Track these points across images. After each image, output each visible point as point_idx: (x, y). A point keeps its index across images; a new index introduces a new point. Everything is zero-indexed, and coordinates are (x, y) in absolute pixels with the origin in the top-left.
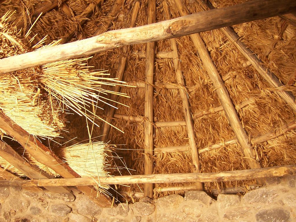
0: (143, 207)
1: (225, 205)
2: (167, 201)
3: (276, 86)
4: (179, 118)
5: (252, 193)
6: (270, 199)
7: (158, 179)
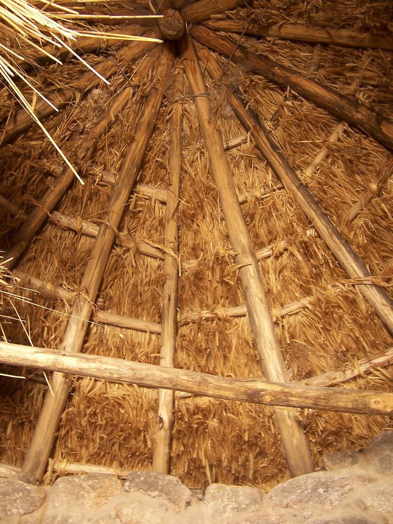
0: (16, 491)
1: (224, 507)
2: (81, 486)
3: (361, 275)
4: (148, 314)
5: (290, 484)
6: (334, 496)
7: (105, 366)
